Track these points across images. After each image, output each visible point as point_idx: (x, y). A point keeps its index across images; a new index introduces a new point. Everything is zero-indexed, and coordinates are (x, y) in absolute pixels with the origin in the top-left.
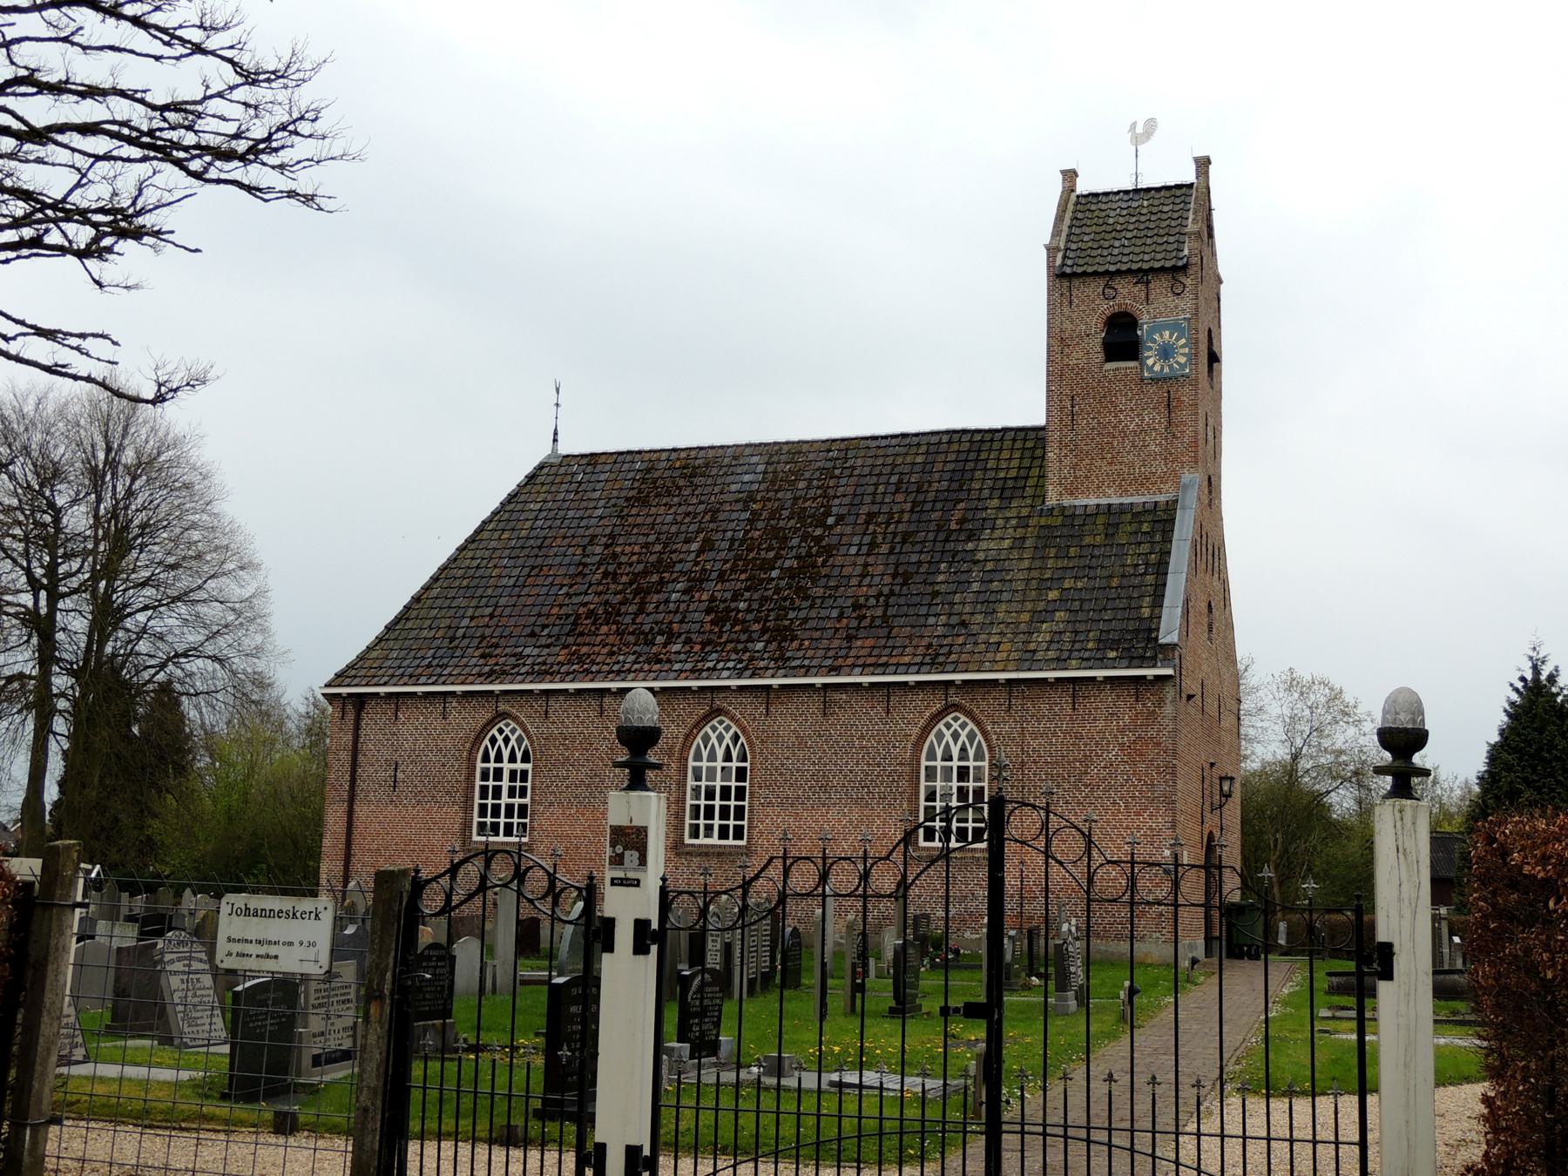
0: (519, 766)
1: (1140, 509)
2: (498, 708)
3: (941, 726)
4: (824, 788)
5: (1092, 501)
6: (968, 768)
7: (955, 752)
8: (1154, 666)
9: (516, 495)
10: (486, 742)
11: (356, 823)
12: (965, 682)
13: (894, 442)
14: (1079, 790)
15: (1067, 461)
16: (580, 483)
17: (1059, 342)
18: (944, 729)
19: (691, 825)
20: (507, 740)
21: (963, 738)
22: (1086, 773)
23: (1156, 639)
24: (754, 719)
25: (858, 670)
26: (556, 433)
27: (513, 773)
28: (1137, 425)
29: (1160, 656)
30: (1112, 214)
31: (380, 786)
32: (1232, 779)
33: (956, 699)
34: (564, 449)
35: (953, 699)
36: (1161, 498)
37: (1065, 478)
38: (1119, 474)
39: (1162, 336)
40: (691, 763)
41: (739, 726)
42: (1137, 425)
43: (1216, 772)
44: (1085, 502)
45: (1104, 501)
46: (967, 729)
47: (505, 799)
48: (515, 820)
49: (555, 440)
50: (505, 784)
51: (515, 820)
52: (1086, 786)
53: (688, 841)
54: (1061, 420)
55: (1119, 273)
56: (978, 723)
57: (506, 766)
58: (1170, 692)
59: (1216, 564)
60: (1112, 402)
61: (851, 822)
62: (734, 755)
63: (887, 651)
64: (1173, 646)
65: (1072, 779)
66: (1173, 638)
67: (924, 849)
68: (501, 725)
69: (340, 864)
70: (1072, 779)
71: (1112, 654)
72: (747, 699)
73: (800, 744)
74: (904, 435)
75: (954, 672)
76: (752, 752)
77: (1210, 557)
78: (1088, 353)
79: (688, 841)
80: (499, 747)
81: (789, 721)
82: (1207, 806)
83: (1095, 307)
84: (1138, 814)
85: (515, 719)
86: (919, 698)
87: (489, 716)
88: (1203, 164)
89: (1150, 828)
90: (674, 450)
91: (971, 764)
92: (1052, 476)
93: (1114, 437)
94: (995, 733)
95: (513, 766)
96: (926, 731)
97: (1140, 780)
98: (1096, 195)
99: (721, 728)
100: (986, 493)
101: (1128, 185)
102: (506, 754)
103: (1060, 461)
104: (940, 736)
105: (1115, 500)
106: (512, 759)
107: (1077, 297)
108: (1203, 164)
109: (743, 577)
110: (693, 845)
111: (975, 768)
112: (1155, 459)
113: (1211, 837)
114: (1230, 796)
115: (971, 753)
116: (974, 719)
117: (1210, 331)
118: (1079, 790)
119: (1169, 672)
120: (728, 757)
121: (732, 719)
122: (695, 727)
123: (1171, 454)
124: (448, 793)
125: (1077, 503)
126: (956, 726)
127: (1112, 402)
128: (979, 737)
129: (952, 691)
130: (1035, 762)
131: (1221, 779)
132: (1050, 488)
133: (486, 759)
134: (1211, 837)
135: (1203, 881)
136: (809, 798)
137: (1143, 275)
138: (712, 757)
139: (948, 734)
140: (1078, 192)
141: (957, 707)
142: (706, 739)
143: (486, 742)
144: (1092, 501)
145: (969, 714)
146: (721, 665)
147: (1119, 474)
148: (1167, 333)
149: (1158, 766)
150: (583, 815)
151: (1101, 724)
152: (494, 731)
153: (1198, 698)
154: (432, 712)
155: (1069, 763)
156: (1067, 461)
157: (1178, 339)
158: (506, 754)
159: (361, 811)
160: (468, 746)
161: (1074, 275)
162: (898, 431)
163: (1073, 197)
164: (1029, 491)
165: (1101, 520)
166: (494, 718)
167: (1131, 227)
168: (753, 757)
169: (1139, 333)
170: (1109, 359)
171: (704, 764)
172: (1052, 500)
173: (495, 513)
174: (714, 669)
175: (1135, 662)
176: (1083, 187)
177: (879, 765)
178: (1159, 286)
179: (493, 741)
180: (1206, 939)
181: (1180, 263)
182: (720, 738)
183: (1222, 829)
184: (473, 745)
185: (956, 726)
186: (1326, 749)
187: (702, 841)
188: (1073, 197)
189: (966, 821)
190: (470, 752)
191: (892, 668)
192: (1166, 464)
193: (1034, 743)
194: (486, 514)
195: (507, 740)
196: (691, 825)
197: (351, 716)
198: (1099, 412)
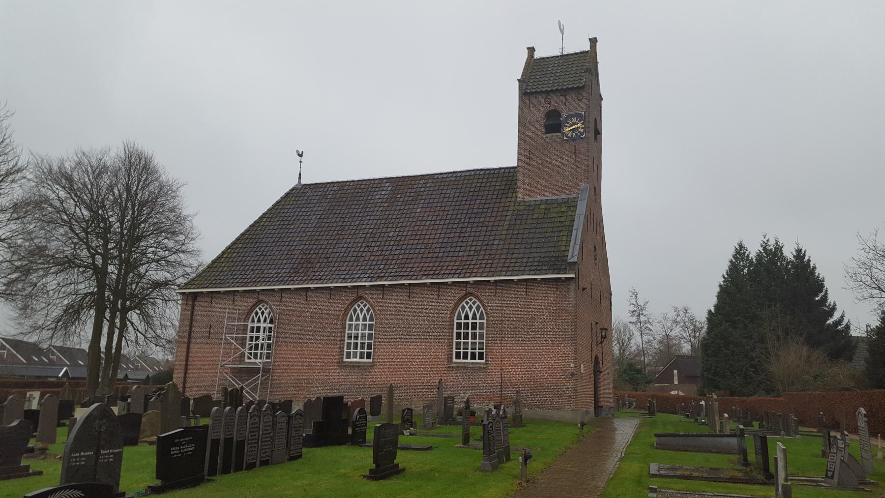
1: (561, 201)
2: (259, 298)
6: (476, 323)
7: (470, 315)
8: (565, 273)
9: (280, 202)
10: (253, 314)
11: (191, 354)
12: (475, 281)
13: (450, 175)
14: (529, 334)
15: (527, 180)
16: (309, 196)
18: (465, 305)
19: (347, 352)
20: (263, 313)
21: (365, 311)
22: (532, 325)
23: (567, 260)
24: (377, 301)
25: (425, 277)
26: (300, 175)
30: (551, 66)
32: (606, 329)
33: (470, 290)
34: (303, 182)
35: (468, 290)
37: (526, 188)
40: (348, 322)
41: (370, 304)
43: (599, 326)
44: (535, 199)
46: (476, 305)
49: (300, 178)
53: (345, 360)
55: (552, 91)
56: (481, 302)
58: (572, 286)
59: (598, 229)
61: (421, 350)
62: (368, 318)
63: (440, 268)
64: (575, 263)
65: (526, 329)
66: (575, 259)
67: (455, 363)
68: (260, 306)
69: (182, 374)
70: (526, 329)
71: (546, 268)
73: (398, 312)
74: (454, 172)
75: (469, 277)
76: (376, 316)
77: (595, 225)
79: (345, 360)
80: (259, 317)
81: (392, 302)
82: (594, 343)
84: (558, 346)
87: (254, 302)
88: (593, 42)
89: (564, 353)
90: (353, 181)
91: (478, 321)
93: (549, 168)
98: (544, 58)
101: (558, 54)
103: (524, 180)
104: (463, 308)
108: (593, 42)
111: (480, 323)
113: (596, 358)
114: (605, 338)
116: (479, 300)
117: (596, 119)
118: (529, 334)
119: (573, 276)
120: (365, 319)
122: (349, 305)
123: (576, 175)
125: (531, 199)
128: (482, 308)
129: (468, 286)
130: (508, 320)
131: (601, 329)
134: (596, 358)
135: (593, 379)
136: (401, 339)
137: (564, 92)
138: (358, 319)
139: (467, 307)
140: (535, 57)
141: (471, 294)
142: (355, 311)
143: (253, 314)
144: (539, 198)
145: (477, 297)
146: (362, 276)
149: (568, 323)
151: (539, 301)
152: (257, 309)
153: (588, 290)
154: (228, 301)
155: (524, 320)
156: (527, 180)
159: (193, 348)
160: (244, 316)
161: (531, 93)
162: (451, 170)
163: (533, 61)
165: (543, 206)
167: (559, 71)
168: (376, 319)
169: (561, 119)
170: (547, 132)
171: (354, 323)
173: (269, 210)
174: (359, 278)
175: (555, 272)
176: (537, 55)
177: (434, 322)
178: (571, 97)
179: (257, 313)
180: (594, 407)
181: (581, 85)
182: (362, 310)
183: (602, 354)
184: (247, 316)
186: (576, 140)
187: (352, 360)
188: (533, 61)
191: (441, 276)
192: (573, 180)
193: (508, 311)
194: (265, 210)
195: (263, 313)
196: (347, 352)
197: (190, 303)
198: (542, 157)
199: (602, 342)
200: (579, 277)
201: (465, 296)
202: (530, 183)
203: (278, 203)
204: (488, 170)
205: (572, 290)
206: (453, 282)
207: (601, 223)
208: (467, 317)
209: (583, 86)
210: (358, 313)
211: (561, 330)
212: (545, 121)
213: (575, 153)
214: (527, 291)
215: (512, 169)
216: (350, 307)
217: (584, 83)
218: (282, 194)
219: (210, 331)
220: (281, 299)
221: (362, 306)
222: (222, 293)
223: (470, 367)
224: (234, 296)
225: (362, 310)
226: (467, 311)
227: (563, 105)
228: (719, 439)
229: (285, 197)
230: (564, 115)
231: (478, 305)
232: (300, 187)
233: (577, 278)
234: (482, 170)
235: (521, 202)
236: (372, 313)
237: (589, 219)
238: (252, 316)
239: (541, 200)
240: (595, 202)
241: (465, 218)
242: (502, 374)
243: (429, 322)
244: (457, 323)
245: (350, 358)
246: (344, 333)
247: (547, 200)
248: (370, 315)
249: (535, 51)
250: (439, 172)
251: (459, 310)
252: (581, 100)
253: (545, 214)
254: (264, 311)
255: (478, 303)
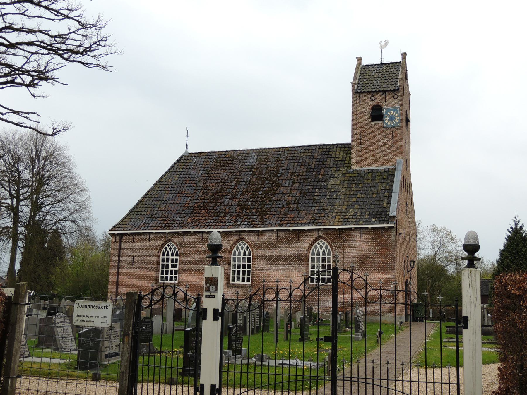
0: (175, 257)
1: (383, 171)
2: (168, 238)
3: (316, 244)
4: (277, 265)
5: (367, 168)
6: (325, 258)
7: (321, 252)
8: (388, 224)
10: (164, 249)
11: (120, 276)
12: (324, 229)
13: (300, 148)
15: (358, 155)
16: (195, 162)
17: (356, 115)
18: (317, 245)
21: (324, 248)
22: (365, 259)
23: (389, 214)
25: (288, 225)
26: (187, 146)
27: (173, 260)
28: (382, 143)
29: (390, 220)
30: (374, 72)
31: (128, 264)
33: (321, 235)
34: (189, 151)
35: (320, 235)
36: (390, 167)
37: (358, 160)
38: (376, 159)
39: (390, 113)
40: (232, 256)
41: (249, 244)
42: (382, 143)
44: (364, 168)
45: (371, 168)
47: (170, 269)
48: (173, 276)
49: (187, 148)
50: (170, 263)
51: (173, 276)
52: (365, 264)
53: (231, 282)
54: (357, 141)
56: (329, 243)
57: (170, 257)
58: (393, 232)
59: (409, 189)
60: (373, 135)
63: (298, 219)
64: (394, 217)
65: (360, 262)
66: (394, 214)
67: (311, 285)
68: (169, 243)
71: (374, 220)
72: (251, 235)
73: (269, 250)
76: (253, 252)
77: (406, 187)
78: (366, 119)
79: (231, 282)
81: (265, 242)
82: (406, 271)
83: (368, 103)
84: (382, 273)
85: (173, 242)
86: (309, 235)
87: (164, 240)
88: (404, 55)
89: (387, 278)
90: (227, 151)
91: (326, 256)
92: (354, 160)
94: (335, 246)
95: (173, 257)
96: (311, 245)
97: (383, 262)
98: (368, 66)
99: (242, 245)
100: (331, 166)
101: (379, 62)
102: (170, 253)
103: (356, 155)
104: (316, 247)
105: (375, 168)
106: (172, 255)
107: (362, 100)
108: (404, 55)
109: (250, 194)
110: (233, 284)
112: (388, 154)
113: (407, 281)
114: (413, 267)
115: (326, 253)
116: (327, 242)
117: (406, 111)
119: (393, 225)
120: (245, 254)
121: (246, 241)
122: (234, 244)
123: (393, 152)
124: (151, 266)
125: (362, 169)
126: (321, 244)
127: (373, 135)
128: (329, 247)
129: (320, 232)
130: (348, 256)
131: (410, 261)
132: (353, 164)
133: (163, 255)
134: (407, 281)
136: (272, 268)
137: (384, 93)
139: (319, 246)
142: (237, 248)
143: (164, 249)
145: (326, 240)
146: (242, 223)
147: (376, 159)
148: (392, 112)
149: (389, 257)
150: (196, 274)
151: (370, 243)
152: (166, 246)
153: (402, 234)
156: (358, 155)
157: (396, 114)
158: (170, 253)
159: (122, 272)
160: (157, 250)
161: (361, 92)
164: (346, 165)
165: (370, 175)
166: (166, 241)
167: (380, 76)
168: (253, 254)
169: (383, 112)
170: (372, 121)
171: (237, 257)
172: (353, 168)
173: (166, 173)
174: (240, 225)
175: (381, 222)
176: (364, 63)
177: (295, 257)
179: (166, 249)
181: (396, 89)
182: (242, 248)
185: (321, 244)
187: (236, 282)
189: (325, 276)
190: (158, 253)
192: (392, 156)
193: (347, 249)
194: (163, 173)
197: (118, 240)
199: (410, 271)
200: (397, 226)
201: (317, 239)
202: (361, 157)
203: (172, 167)
204: (329, 145)
205: (392, 235)
206: (309, 229)
207: (410, 185)
208: (319, 254)
209: (398, 90)
210: (318, 249)
211: (385, 263)
212: (371, 112)
213: (393, 136)
214: (361, 236)
215: (346, 145)
216: (233, 245)
217: (398, 87)
218: (175, 160)
219: (133, 261)
220: (184, 239)
221: (242, 245)
222: (141, 234)
223: (321, 288)
224: (150, 236)
225: (242, 248)
226: (318, 249)
227: (383, 102)
228: (487, 328)
229: (177, 163)
230: (385, 110)
231: (327, 245)
232: (187, 155)
233: (396, 226)
234: (324, 145)
235: (354, 171)
236: (250, 250)
237: (403, 184)
238: (233, 251)
239: (369, 170)
240: (406, 170)
241: (314, 182)
242: (343, 293)
243: (292, 257)
244: (162, 264)
245: (234, 281)
246: (230, 264)
247: (373, 170)
248: (328, 251)
249: (362, 59)
250: (292, 145)
251: (313, 249)
252: (396, 99)
253: (372, 180)
254: (171, 247)
255: (326, 244)
